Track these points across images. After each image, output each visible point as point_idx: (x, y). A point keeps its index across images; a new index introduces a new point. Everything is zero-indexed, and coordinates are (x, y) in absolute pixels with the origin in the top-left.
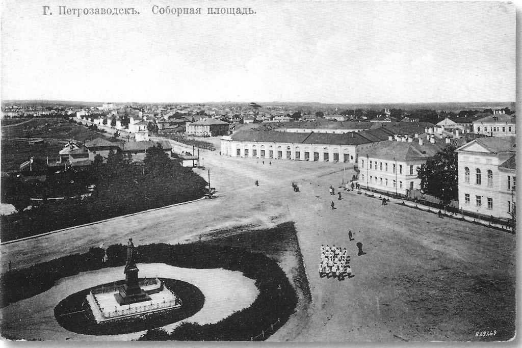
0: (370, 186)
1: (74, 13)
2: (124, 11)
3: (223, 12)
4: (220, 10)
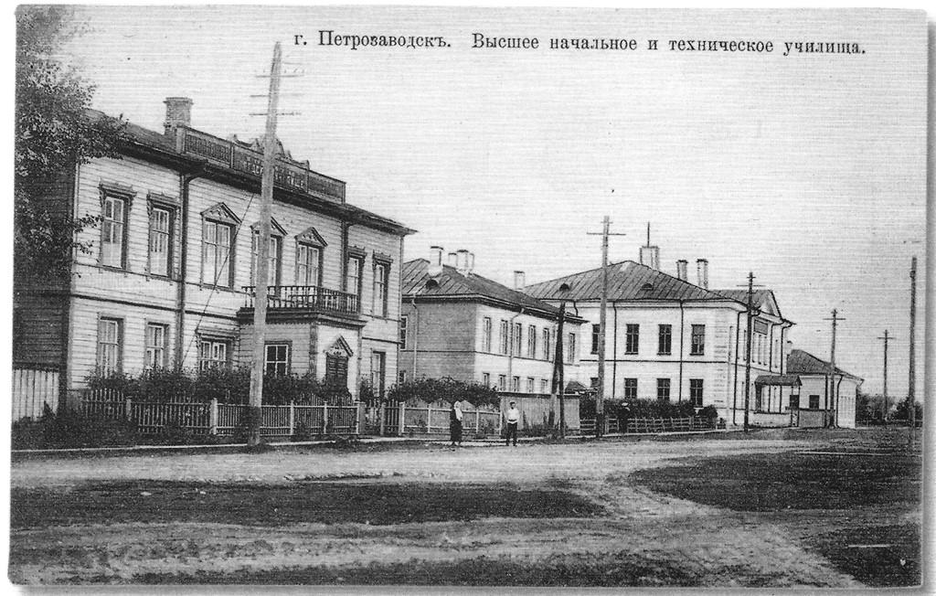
0: (283, 267)
1: (346, 44)
2: (746, 46)
3: (624, 45)
4: (619, 42)
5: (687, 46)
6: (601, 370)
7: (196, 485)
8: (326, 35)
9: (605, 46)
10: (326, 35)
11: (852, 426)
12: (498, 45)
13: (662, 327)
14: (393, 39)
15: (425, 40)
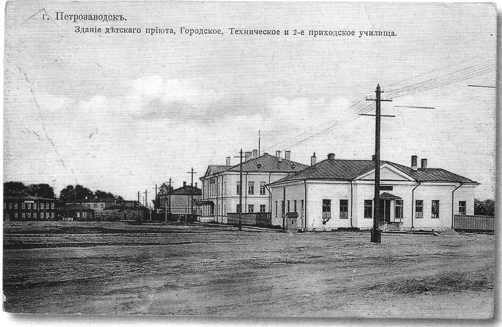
2: (208, 31)
5: (239, 32)
6: (241, 201)
7: (379, 133)
8: (60, 15)
9: (122, 19)
10: (60, 15)
11: (372, 220)
12: (351, 32)
13: (324, 201)
14: (96, 16)
15: (113, 17)
